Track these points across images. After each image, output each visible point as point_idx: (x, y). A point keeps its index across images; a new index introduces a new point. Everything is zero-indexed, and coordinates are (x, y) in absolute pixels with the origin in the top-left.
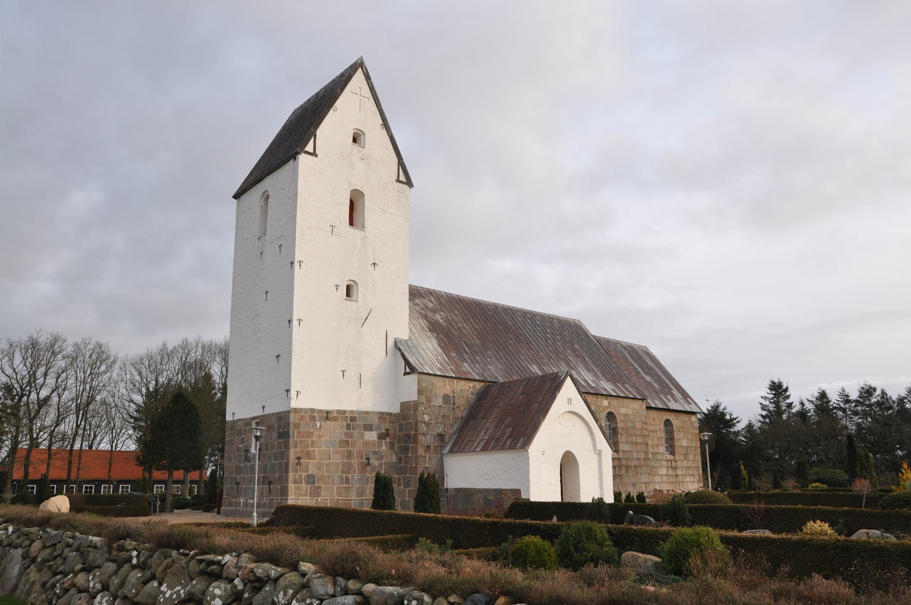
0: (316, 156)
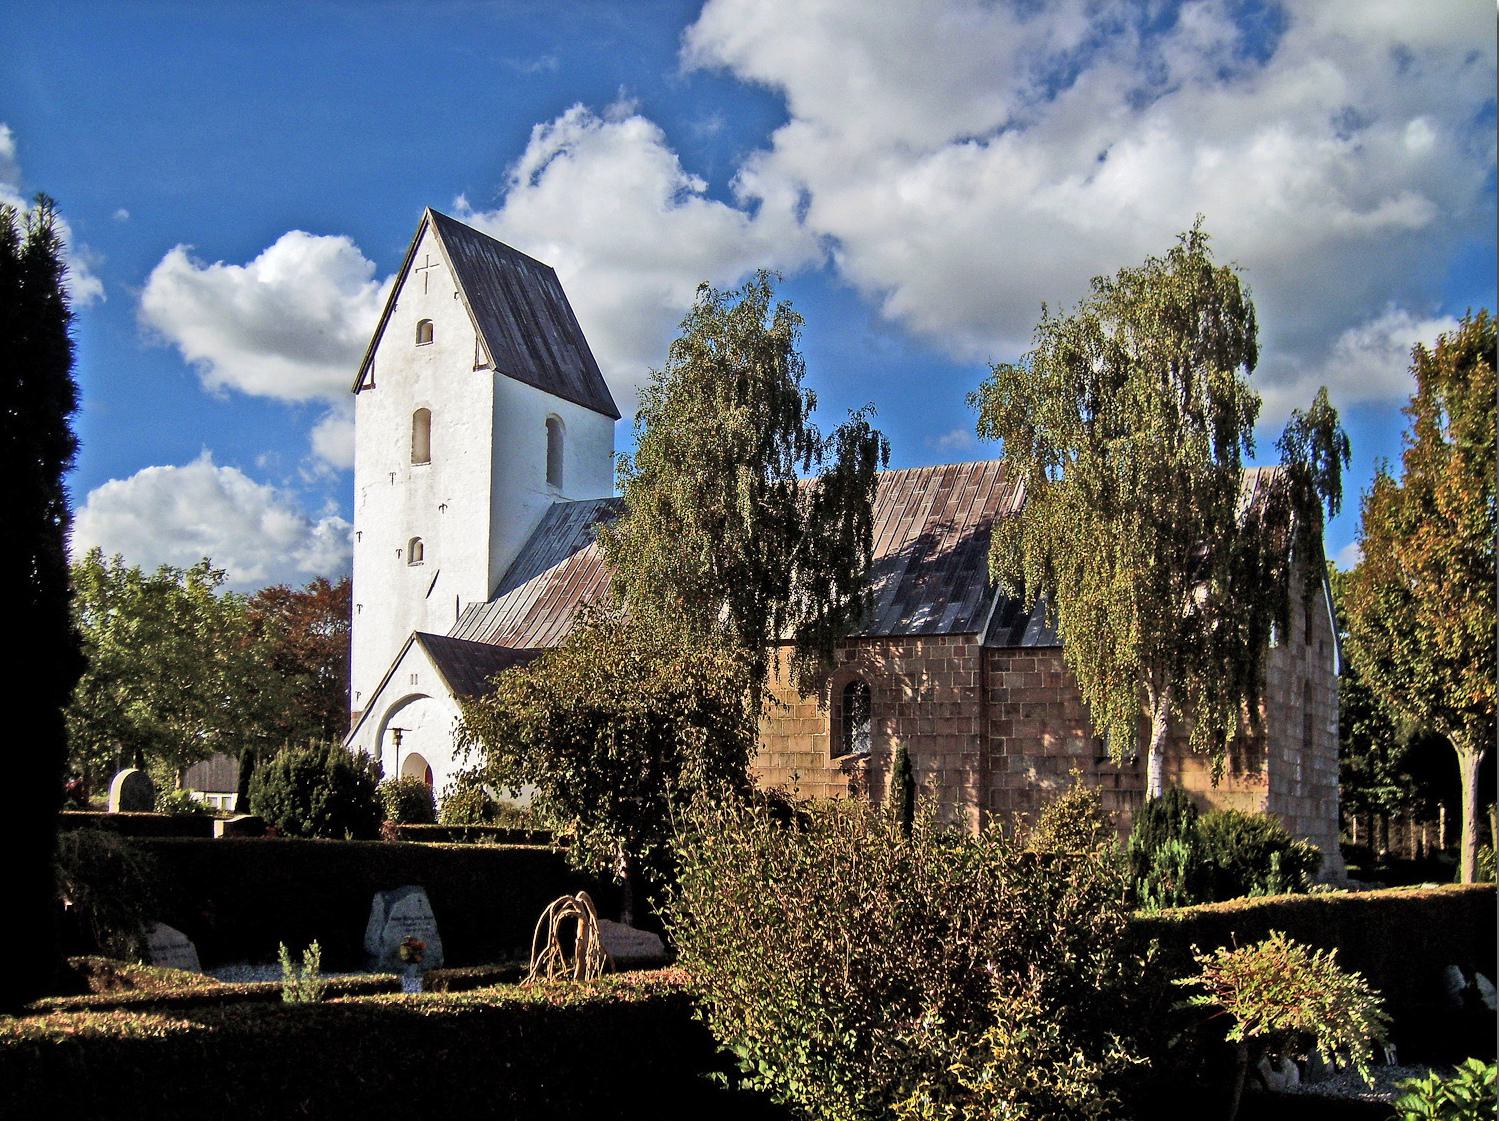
0: (474, 369)
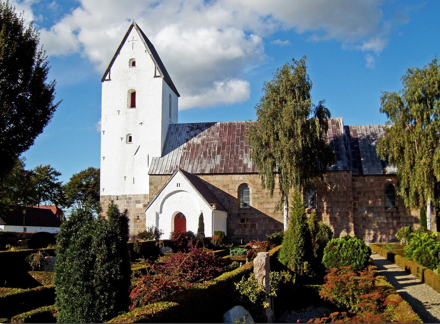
0: (154, 77)
